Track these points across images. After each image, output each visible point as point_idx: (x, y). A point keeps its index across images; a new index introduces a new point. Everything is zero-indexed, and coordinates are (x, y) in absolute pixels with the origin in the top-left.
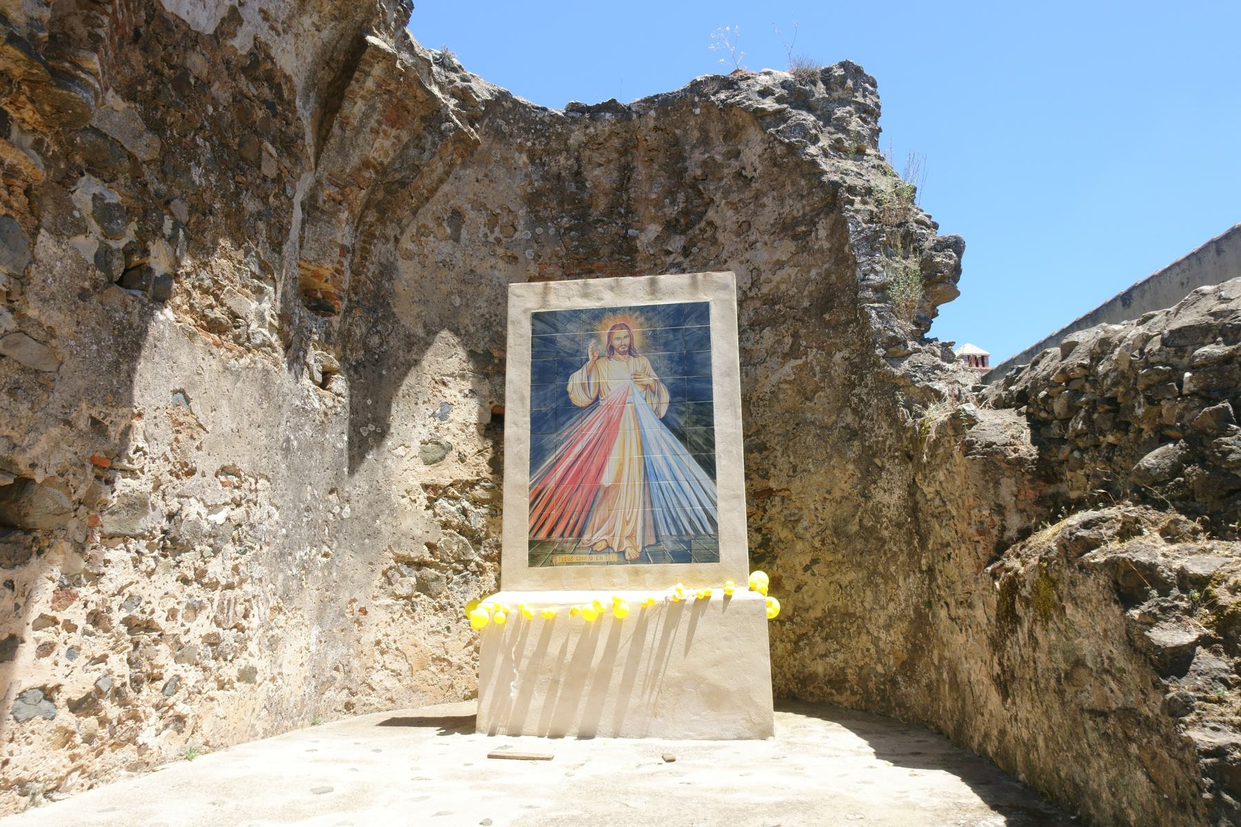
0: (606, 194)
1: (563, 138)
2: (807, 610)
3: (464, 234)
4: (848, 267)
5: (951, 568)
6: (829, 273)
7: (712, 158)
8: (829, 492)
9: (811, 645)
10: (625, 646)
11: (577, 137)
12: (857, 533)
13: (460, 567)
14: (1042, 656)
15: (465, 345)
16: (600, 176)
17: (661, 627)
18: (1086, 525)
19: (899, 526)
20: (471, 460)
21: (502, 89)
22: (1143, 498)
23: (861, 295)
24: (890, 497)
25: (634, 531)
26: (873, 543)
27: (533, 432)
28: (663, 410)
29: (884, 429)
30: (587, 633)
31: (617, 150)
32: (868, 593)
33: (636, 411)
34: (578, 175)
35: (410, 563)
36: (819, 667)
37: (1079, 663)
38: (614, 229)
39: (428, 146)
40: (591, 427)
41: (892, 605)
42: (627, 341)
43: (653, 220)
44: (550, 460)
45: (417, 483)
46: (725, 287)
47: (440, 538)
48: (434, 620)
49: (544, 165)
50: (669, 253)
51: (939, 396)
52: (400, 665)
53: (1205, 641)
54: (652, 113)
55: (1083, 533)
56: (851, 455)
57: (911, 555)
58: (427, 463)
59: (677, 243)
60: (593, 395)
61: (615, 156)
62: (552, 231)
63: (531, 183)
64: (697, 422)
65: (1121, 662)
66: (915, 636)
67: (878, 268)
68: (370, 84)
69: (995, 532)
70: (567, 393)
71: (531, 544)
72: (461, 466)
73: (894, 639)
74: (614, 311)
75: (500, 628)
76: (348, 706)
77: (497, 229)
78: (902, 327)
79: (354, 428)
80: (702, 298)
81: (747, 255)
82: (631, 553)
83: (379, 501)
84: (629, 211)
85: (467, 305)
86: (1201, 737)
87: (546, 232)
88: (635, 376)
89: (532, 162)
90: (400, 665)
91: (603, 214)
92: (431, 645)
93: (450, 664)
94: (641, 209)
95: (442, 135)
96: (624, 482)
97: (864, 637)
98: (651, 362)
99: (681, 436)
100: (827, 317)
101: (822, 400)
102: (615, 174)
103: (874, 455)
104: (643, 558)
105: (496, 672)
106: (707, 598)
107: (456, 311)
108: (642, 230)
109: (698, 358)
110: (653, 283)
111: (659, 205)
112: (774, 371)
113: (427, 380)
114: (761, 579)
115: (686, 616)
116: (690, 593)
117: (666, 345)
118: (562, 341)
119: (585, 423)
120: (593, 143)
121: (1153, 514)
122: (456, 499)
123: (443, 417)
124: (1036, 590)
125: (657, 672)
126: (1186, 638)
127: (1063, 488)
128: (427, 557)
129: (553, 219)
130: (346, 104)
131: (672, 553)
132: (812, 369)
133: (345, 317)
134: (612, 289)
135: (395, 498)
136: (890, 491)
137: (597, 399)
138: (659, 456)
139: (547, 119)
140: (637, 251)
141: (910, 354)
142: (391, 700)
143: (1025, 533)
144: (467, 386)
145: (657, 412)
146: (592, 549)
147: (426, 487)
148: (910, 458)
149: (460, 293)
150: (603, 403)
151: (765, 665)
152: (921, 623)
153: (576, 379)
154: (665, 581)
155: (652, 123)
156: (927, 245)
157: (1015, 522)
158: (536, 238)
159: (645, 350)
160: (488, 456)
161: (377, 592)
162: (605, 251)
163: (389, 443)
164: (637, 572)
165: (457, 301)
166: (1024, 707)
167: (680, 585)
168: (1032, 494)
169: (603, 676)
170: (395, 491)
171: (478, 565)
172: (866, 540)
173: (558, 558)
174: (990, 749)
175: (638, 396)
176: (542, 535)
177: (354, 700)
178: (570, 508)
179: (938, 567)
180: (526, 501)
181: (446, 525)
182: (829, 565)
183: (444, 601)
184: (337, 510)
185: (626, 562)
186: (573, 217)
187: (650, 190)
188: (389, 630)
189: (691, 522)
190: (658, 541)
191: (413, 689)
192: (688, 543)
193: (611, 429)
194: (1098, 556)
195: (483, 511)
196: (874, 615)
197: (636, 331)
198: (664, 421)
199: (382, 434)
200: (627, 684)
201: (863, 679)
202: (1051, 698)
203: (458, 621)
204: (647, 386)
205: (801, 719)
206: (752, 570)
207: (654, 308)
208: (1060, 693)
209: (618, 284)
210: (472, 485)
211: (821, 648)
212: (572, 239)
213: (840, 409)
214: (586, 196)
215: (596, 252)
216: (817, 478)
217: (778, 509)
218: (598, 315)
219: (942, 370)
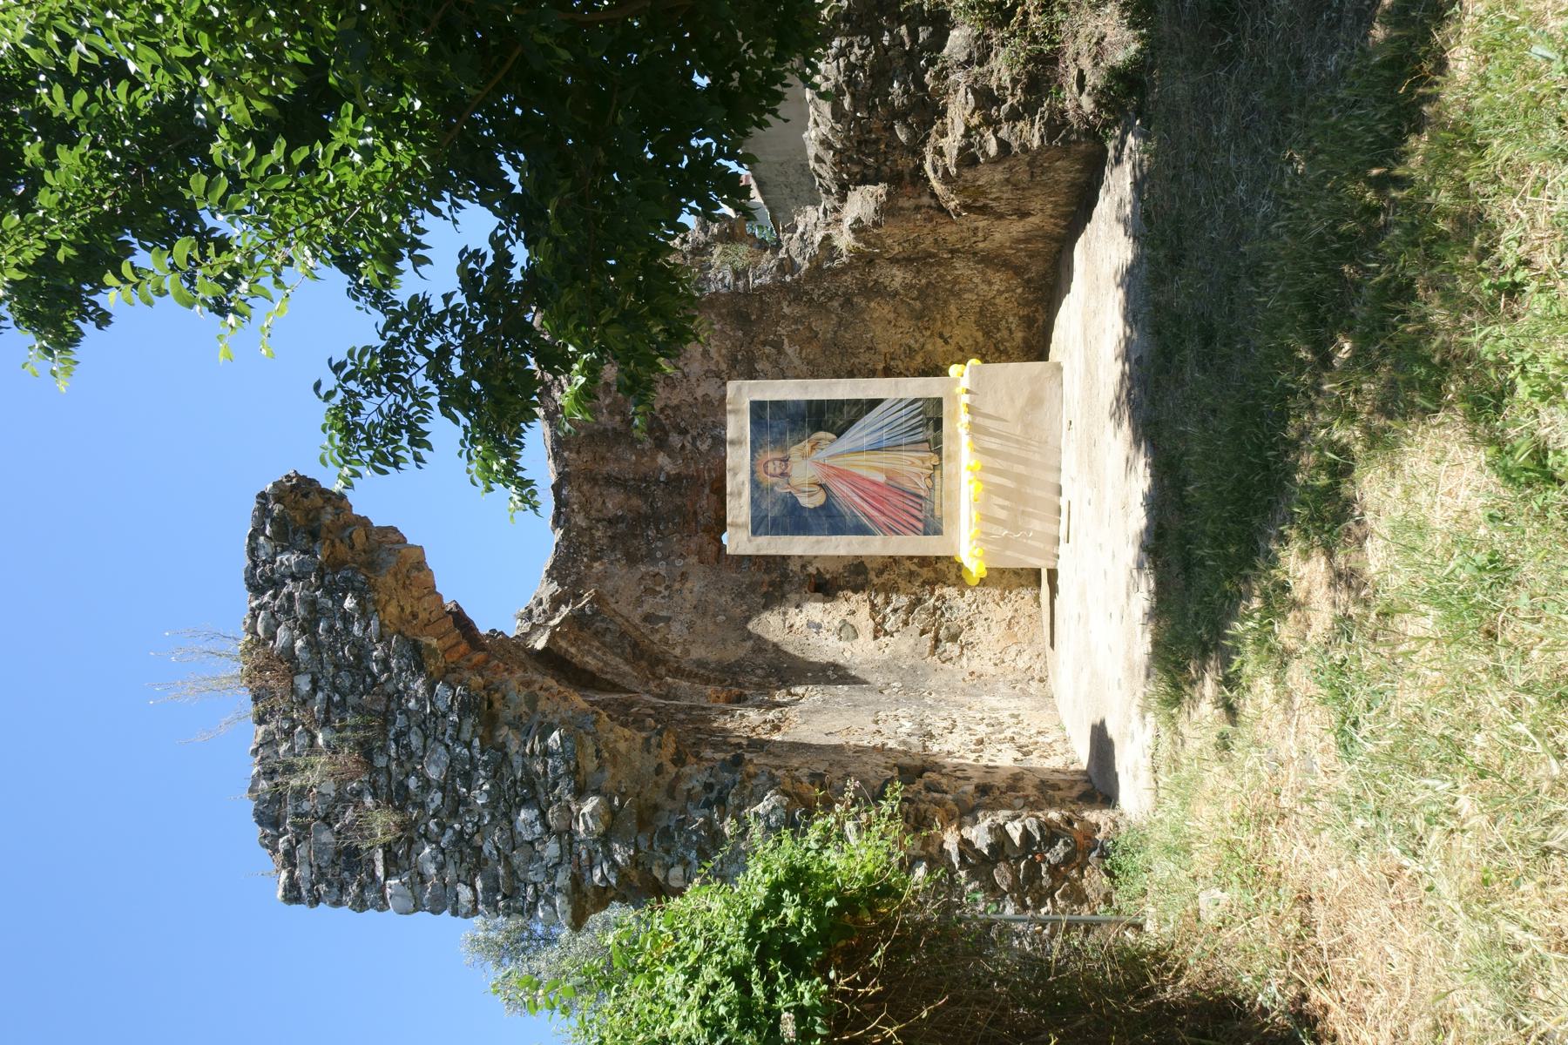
0: (629, 498)
1: (581, 532)
2: (977, 343)
3: (664, 613)
4: (717, 299)
5: (952, 239)
6: (719, 315)
7: (608, 406)
8: (890, 322)
9: (1003, 341)
10: (999, 464)
11: (580, 520)
12: (922, 303)
13: (939, 612)
14: (1005, 196)
15: (759, 613)
16: (613, 503)
17: (986, 438)
18: (936, 172)
19: (919, 271)
20: (853, 606)
21: (544, 575)
22: (923, 143)
23: (741, 291)
24: (898, 277)
25: (918, 458)
26: (930, 291)
27: (843, 533)
28: (831, 436)
29: (847, 279)
30: (991, 490)
31: (592, 487)
32: (965, 296)
33: (831, 457)
34: (612, 522)
35: (936, 647)
36: (1019, 335)
37: (1007, 180)
38: (659, 493)
39: (604, 625)
40: (841, 489)
41: (975, 280)
42: (777, 463)
43: (654, 459)
44: (865, 520)
45: (873, 643)
46: (739, 389)
47: (916, 627)
48: (979, 630)
49: (602, 550)
50: (683, 447)
51: (827, 238)
52: (1013, 650)
53: (995, 133)
54: (566, 454)
55: (940, 174)
56: (863, 304)
57: (940, 265)
58: (856, 636)
59: (675, 440)
60: (817, 488)
61: (597, 489)
62: (659, 544)
63: (618, 560)
64: (841, 411)
65: (1007, 165)
66: (997, 265)
67: (720, 276)
68: (573, 650)
69: (931, 212)
70: (815, 509)
71: (926, 534)
72: (858, 614)
73: (998, 279)
74: (753, 472)
75: (986, 553)
76: (1041, 680)
77: (658, 589)
78: (768, 261)
79: (829, 682)
80: (747, 406)
81: (693, 380)
82: (935, 460)
83: (887, 667)
84: (644, 479)
85: (725, 610)
86: (1036, 143)
87: (660, 549)
88: (804, 457)
89: (600, 559)
90: (1013, 650)
91: (646, 502)
92: (998, 631)
93: (1013, 617)
94: (643, 469)
95: (596, 613)
96: (883, 466)
97: (997, 301)
98: (794, 444)
99: (851, 423)
100: (753, 317)
101: (818, 325)
102: (612, 490)
103: (866, 287)
104: (939, 452)
105: (1017, 555)
106: (968, 405)
107: (729, 619)
108: (662, 469)
109: (792, 410)
110: (733, 443)
111: (643, 453)
112: (791, 362)
113: (790, 638)
114: (954, 370)
115: (979, 420)
116: (964, 418)
117: (782, 433)
118: (774, 512)
119: (838, 494)
120: (585, 506)
121: (932, 140)
122: (884, 617)
123: (819, 626)
124: (969, 197)
125: (1017, 441)
126: (993, 141)
127: (907, 171)
128: (932, 635)
129: (648, 543)
130: (589, 667)
131: (935, 431)
132: (792, 331)
133: (745, 688)
134: (735, 474)
135: (885, 657)
136: (893, 277)
137: (820, 485)
138: (865, 440)
139: (566, 543)
140: (679, 474)
141: (790, 256)
142: (1038, 656)
143: (934, 195)
144: (792, 611)
145: (832, 441)
146: (931, 489)
147: (876, 638)
148: (872, 261)
149: (715, 616)
150: (824, 481)
151: (1013, 366)
152: (990, 260)
153: (806, 501)
154: (955, 436)
155: (574, 455)
156: (702, 237)
157: (926, 200)
158: (666, 558)
159: (784, 449)
160: (850, 593)
161: (957, 667)
162: (678, 501)
163: (841, 662)
164: (949, 456)
165: (721, 618)
166: (1035, 205)
167: (958, 425)
168: (909, 189)
169: (1019, 478)
170: (878, 656)
171: (937, 600)
172: (928, 295)
173: (937, 513)
174: (1063, 223)
175: (820, 455)
176: (920, 526)
177: (1037, 678)
178: (900, 505)
179: (950, 246)
180: (895, 538)
181: (906, 623)
182: (944, 325)
183: (965, 623)
184: (896, 690)
185: (941, 464)
186: (648, 526)
187: (628, 460)
188: (987, 658)
189: (913, 418)
190: (927, 441)
191: (1031, 642)
192: (929, 419)
193: (842, 474)
194: (953, 171)
195: (894, 597)
196: (981, 293)
197: (770, 456)
198: (839, 436)
199: (835, 666)
200: (1025, 462)
201: (1027, 303)
202: (1027, 194)
203: (980, 613)
204: (813, 448)
205: (1053, 347)
206: (948, 375)
207: (752, 442)
208: (1024, 189)
209: (732, 469)
210: (873, 606)
211: (1005, 333)
212: (667, 527)
213: (828, 311)
214: (630, 515)
215: (678, 508)
216: (878, 330)
217: (900, 363)
218: (755, 485)
219: (803, 234)
